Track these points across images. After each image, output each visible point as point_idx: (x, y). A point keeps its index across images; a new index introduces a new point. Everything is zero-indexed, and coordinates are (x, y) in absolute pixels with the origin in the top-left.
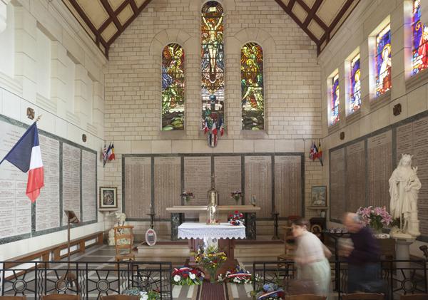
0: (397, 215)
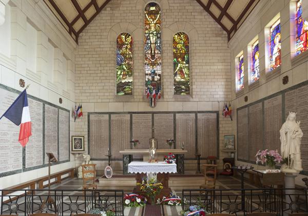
0: (286, 156)
